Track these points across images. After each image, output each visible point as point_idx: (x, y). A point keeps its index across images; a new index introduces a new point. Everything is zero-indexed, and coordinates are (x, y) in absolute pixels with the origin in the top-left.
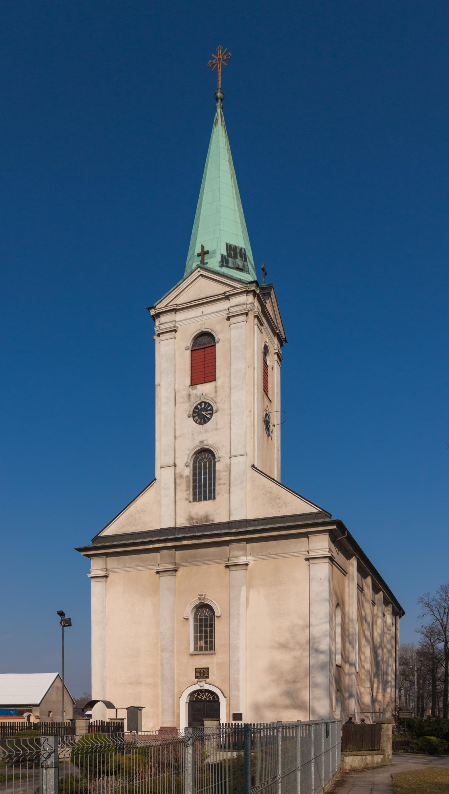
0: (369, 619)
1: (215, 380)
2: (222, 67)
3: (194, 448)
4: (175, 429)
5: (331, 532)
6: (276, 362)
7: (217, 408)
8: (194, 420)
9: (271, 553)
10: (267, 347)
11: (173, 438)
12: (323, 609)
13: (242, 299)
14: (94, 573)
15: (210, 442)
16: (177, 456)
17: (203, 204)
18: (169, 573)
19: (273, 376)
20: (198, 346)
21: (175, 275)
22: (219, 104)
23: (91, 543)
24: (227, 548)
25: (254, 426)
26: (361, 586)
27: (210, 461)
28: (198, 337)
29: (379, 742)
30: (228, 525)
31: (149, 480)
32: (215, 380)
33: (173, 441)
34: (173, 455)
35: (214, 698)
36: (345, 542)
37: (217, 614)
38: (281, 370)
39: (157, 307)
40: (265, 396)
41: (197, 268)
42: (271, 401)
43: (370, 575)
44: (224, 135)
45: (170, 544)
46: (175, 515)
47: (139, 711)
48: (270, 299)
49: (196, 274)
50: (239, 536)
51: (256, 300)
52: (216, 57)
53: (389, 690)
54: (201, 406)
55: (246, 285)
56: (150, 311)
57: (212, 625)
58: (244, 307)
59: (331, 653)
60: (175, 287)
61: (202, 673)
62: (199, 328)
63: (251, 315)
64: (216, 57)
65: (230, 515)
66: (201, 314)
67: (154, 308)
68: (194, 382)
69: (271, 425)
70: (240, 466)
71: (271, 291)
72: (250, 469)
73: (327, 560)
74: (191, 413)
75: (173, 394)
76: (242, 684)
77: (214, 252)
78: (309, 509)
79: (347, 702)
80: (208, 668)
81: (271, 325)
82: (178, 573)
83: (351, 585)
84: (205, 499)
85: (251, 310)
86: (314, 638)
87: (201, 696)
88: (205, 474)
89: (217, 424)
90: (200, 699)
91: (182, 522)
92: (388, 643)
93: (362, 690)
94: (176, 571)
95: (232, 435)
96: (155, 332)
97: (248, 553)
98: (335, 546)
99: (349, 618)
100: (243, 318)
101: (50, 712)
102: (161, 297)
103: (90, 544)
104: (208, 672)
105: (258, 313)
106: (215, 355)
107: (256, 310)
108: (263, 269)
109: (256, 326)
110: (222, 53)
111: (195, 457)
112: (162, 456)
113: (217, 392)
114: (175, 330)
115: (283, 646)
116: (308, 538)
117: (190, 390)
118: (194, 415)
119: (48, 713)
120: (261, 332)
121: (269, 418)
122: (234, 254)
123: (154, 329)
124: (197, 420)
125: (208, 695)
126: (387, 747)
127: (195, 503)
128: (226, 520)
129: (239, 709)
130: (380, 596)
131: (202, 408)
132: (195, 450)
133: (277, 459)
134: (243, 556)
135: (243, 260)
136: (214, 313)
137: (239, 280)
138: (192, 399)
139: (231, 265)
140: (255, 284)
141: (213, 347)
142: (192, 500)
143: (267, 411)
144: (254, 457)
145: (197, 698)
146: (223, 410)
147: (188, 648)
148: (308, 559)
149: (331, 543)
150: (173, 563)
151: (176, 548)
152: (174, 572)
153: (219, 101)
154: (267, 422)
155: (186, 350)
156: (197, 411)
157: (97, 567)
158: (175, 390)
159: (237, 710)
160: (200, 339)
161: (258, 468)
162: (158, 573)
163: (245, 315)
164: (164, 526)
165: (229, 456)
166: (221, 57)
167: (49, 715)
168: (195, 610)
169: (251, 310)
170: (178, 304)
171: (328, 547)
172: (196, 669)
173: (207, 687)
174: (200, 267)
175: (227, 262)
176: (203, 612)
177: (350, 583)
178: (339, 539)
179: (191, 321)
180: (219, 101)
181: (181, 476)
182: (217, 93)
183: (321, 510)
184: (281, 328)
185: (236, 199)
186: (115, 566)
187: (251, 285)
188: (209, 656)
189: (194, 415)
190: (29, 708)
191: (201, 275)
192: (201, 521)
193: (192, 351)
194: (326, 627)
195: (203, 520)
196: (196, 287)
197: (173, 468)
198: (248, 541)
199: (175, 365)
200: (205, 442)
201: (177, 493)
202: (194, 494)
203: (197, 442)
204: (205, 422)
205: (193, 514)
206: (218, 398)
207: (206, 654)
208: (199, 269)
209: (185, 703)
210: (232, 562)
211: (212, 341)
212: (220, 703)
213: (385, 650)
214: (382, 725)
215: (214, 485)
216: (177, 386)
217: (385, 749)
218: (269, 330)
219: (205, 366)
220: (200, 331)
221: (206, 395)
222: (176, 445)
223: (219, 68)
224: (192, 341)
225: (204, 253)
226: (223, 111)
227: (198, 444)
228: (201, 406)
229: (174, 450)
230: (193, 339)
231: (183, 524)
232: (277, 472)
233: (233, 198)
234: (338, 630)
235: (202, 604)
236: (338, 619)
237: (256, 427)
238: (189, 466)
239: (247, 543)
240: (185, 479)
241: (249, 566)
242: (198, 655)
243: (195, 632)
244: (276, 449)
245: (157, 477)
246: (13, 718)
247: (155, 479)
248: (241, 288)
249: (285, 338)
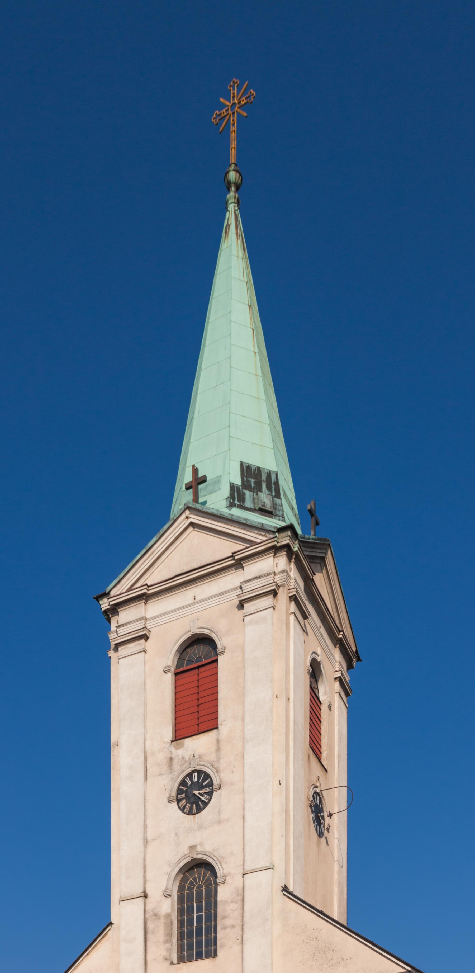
3: (179, 861)
4: (145, 826)
6: (337, 696)
7: (221, 781)
8: (179, 807)
10: (319, 663)
11: (141, 844)
15: (208, 848)
16: (149, 876)
17: (199, 392)
19: (331, 723)
20: (187, 665)
22: (232, 196)
25: (287, 811)
27: (208, 886)
28: (187, 647)
33: (142, 848)
34: (142, 874)
39: (113, 593)
40: (313, 759)
42: (326, 771)
44: (241, 253)
48: (324, 571)
49: (182, 523)
51: (293, 565)
52: (228, 103)
54: (191, 779)
55: (272, 536)
58: (269, 579)
63: (283, 595)
64: (228, 103)
66: (191, 601)
67: (106, 595)
68: (180, 734)
69: (326, 814)
70: (261, 891)
71: (326, 554)
72: (279, 895)
74: (174, 793)
75: (142, 758)
77: (218, 480)
84: (200, 956)
85: (283, 586)
88: (199, 910)
89: (219, 812)
95: (247, 831)
96: (110, 643)
100: (268, 601)
105: (297, 591)
109: (292, 617)
110: (238, 94)
111: (182, 878)
112: (123, 878)
114: (145, 634)
117: (173, 749)
118: (179, 796)
120: (305, 631)
121: (321, 801)
122: (255, 483)
124: (185, 806)
127: (182, 965)
131: (192, 783)
132: (182, 864)
133: (339, 883)
135: (274, 494)
136: (215, 596)
137: (260, 526)
138: (176, 767)
139: (248, 503)
140: (289, 533)
141: (215, 664)
142: (175, 960)
143: (316, 787)
144: (287, 872)
146: (232, 784)
153: (233, 189)
154: (317, 808)
156: (185, 789)
158: (145, 752)
160: (190, 651)
161: (296, 893)
163: (271, 596)
165: (242, 872)
166: (236, 101)
169: (283, 586)
170: (149, 584)
174: (188, 508)
175: (242, 498)
180: (233, 189)
182: (228, 172)
183: (409, 969)
185: (261, 379)
187: (283, 535)
191: (192, 524)
193: (176, 674)
196: (184, 547)
199: (145, 704)
200: (199, 849)
201: (148, 948)
202: (181, 948)
203: (184, 850)
206: (222, 761)
208: (187, 512)
215: (216, 932)
216: (148, 743)
218: (323, 630)
220: (189, 635)
221: (200, 756)
223: (233, 124)
228: (191, 779)
229: (143, 866)
230: (177, 651)
232: (339, 907)
237: (292, 813)
238: (170, 895)
240: (162, 920)
244: (336, 863)
245: (113, 919)
247: (111, 924)
249: (356, 650)
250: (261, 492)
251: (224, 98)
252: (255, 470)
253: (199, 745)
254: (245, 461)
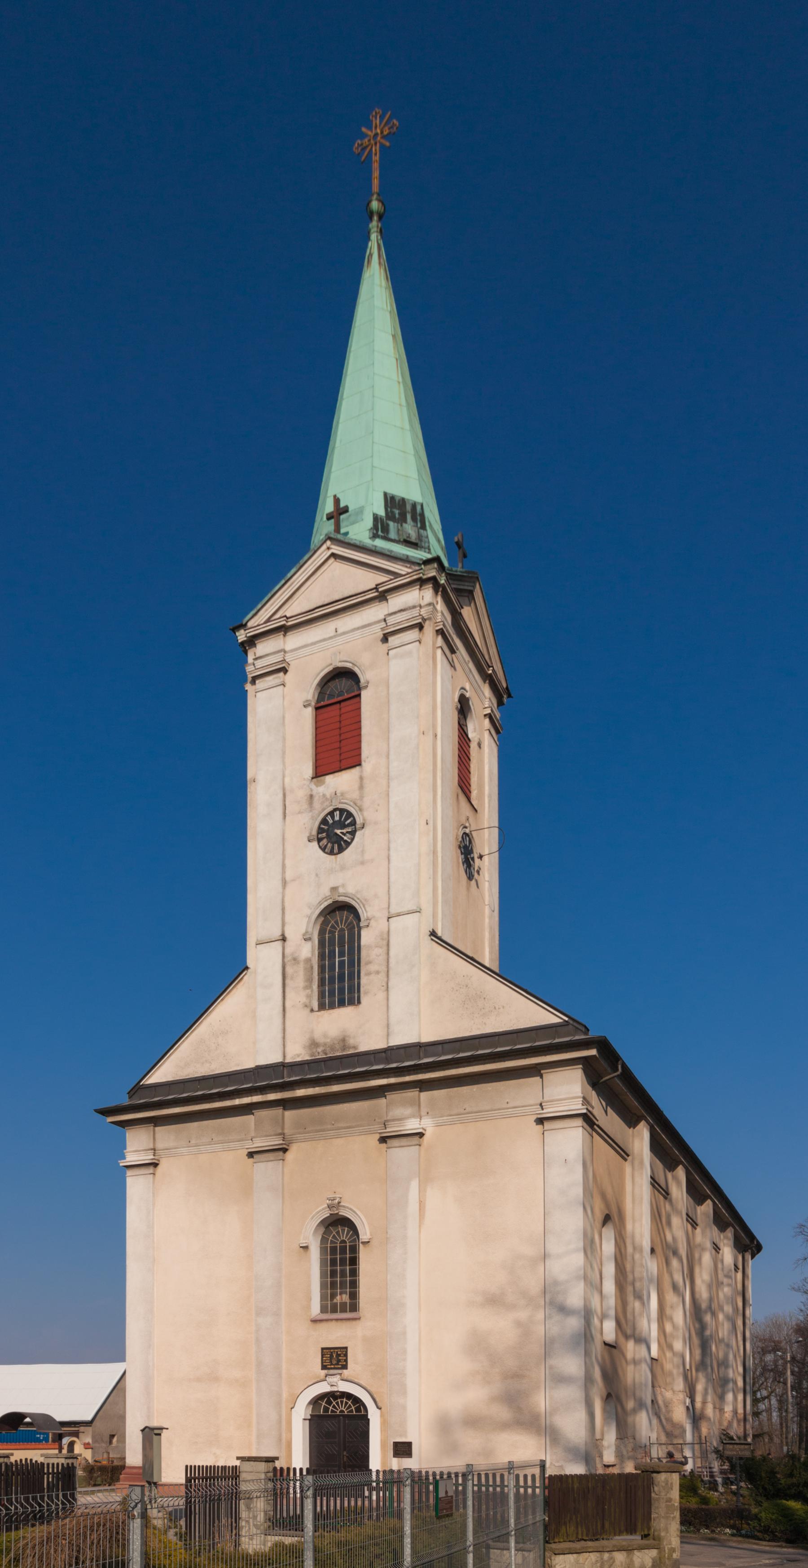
0: (683, 1252)
1: (360, 765)
2: (380, 151)
3: (320, 903)
5: (587, 1064)
6: (486, 734)
7: (364, 820)
8: (320, 847)
9: (467, 1111)
10: (467, 700)
12: (571, 1223)
13: (412, 596)
14: (131, 1158)
15: (351, 889)
16: (288, 918)
18: (271, 1156)
19: (481, 762)
21: (288, 549)
22: (374, 225)
23: (127, 1099)
24: (382, 1101)
25: (435, 852)
26: (664, 1187)
28: (329, 681)
29: (648, 1518)
30: (383, 1054)
31: (235, 968)
32: (360, 765)
33: (281, 890)
35: (358, 1410)
36: (619, 1088)
37: (363, 1237)
38: (499, 752)
39: (250, 624)
40: (462, 798)
41: (325, 542)
43: (681, 1163)
44: (384, 283)
45: (272, 1097)
46: (284, 1038)
47: (155, 1437)
48: (473, 604)
49: (322, 554)
50: (404, 1076)
51: (439, 599)
52: (369, 133)
53: (730, 1397)
54: (333, 817)
55: (417, 568)
56: (237, 634)
57: (354, 1261)
58: (415, 612)
59: (587, 1314)
60: (283, 582)
62: (329, 662)
63: (429, 629)
64: (369, 133)
65: (388, 1035)
66: (333, 633)
67: (243, 626)
68: (320, 771)
69: (476, 856)
70: (408, 934)
71: (474, 587)
72: (426, 940)
73: (579, 1122)
74: (314, 832)
75: (281, 796)
76: (411, 1381)
77: (361, 511)
78: (544, 1017)
79: (630, 1419)
80: (346, 1348)
81: (476, 656)
82: (289, 1156)
83: (637, 1179)
84: (342, 1004)
85: (430, 619)
86: (556, 1283)
87: (334, 1407)
88: (342, 954)
89: (363, 852)
90: (332, 1411)
91: (297, 1052)
92: (728, 1303)
93: (668, 1395)
94: (285, 1150)
95: (392, 872)
97: (423, 1111)
98: (598, 1095)
99: (633, 1243)
100: (413, 634)
101: (112, 1436)
102: (258, 603)
103: (126, 1101)
104: (346, 1355)
105: (444, 625)
106: (359, 715)
107: (439, 618)
108: (459, 545)
109: (439, 652)
110: (380, 123)
112: (260, 920)
113: (370, 793)
114: (284, 668)
115: (494, 1301)
116: (541, 1077)
117: (313, 786)
118: (320, 836)
119: (107, 1439)
121: (470, 842)
122: (399, 514)
123: (245, 671)
124: (326, 846)
125: (346, 1403)
126: (666, 1529)
127: (322, 1012)
128: (381, 1045)
129: (405, 1434)
130: (706, 1208)
131: (334, 822)
132: (323, 907)
133: (491, 928)
134: (414, 1116)
135: (419, 525)
136: (358, 628)
137: (405, 558)
138: (317, 805)
139: (393, 535)
140: (436, 565)
141: (357, 699)
142: (316, 1007)
143: (466, 827)
145: (326, 1410)
146: (376, 823)
147: (308, 1307)
148: (540, 1121)
149: (589, 1088)
150: (280, 1134)
151: (285, 1104)
152: (281, 1153)
153: (375, 218)
154: (466, 850)
155: (305, 706)
156: (326, 827)
157: (137, 1145)
159: (401, 1436)
161: (444, 938)
162: (251, 1155)
163: (417, 630)
164: (263, 1061)
165: (387, 915)
166: (379, 131)
167: (111, 1442)
168: (322, 1230)
169: (430, 619)
170: (288, 615)
171: (580, 1095)
172: (323, 1349)
173: (344, 1387)
174: (330, 538)
175: (386, 529)
176: (338, 1233)
177: (636, 1174)
178: (604, 1079)
179: (315, 648)
180: (375, 218)
181: (295, 960)
183: (566, 1019)
184: (497, 666)
186: (171, 1144)
187: (429, 567)
188: (348, 1324)
189: (320, 836)
190: (74, 1427)
191: (333, 555)
192: (332, 1048)
194: (578, 1259)
195: (337, 1047)
196: (325, 578)
197: (280, 943)
198: (424, 1086)
199: (284, 739)
200: (341, 890)
202: (321, 995)
203: (325, 891)
204: (341, 850)
205: (318, 1036)
207: (341, 1320)
208: (329, 543)
209: (301, 1420)
210: (392, 1129)
211: (355, 687)
212: (369, 1420)
213: (721, 1317)
214: (655, 1475)
215: (359, 977)
216: (287, 780)
217: (663, 1534)
218: (471, 665)
219: (343, 737)
220: (330, 668)
221: (342, 794)
222: (286, 899)
223: (376, 154)
224: (316, 689)
225: (340, 511)
226: (382, 237)
227: (328, 893)
230: (318, 685)
231: (298, 1056)
232: (491, 953)
233: (400, 405)
234: (610, 1269)
235: (335, 1218)
236: (608, 1247)
237: (440, 854)
238: (309, 939)
239: (421, 1091)
240: (302, 965)
241: (425, 1137)
242: (327, 1320)
243: (323, 1275)
245: (249, 963)
246: (41, 1447)
247: (247, 968)
248: (408, 573)
249: (507, 688)
251: (367, 127)
252: (399, 501)
253: (341, 784)
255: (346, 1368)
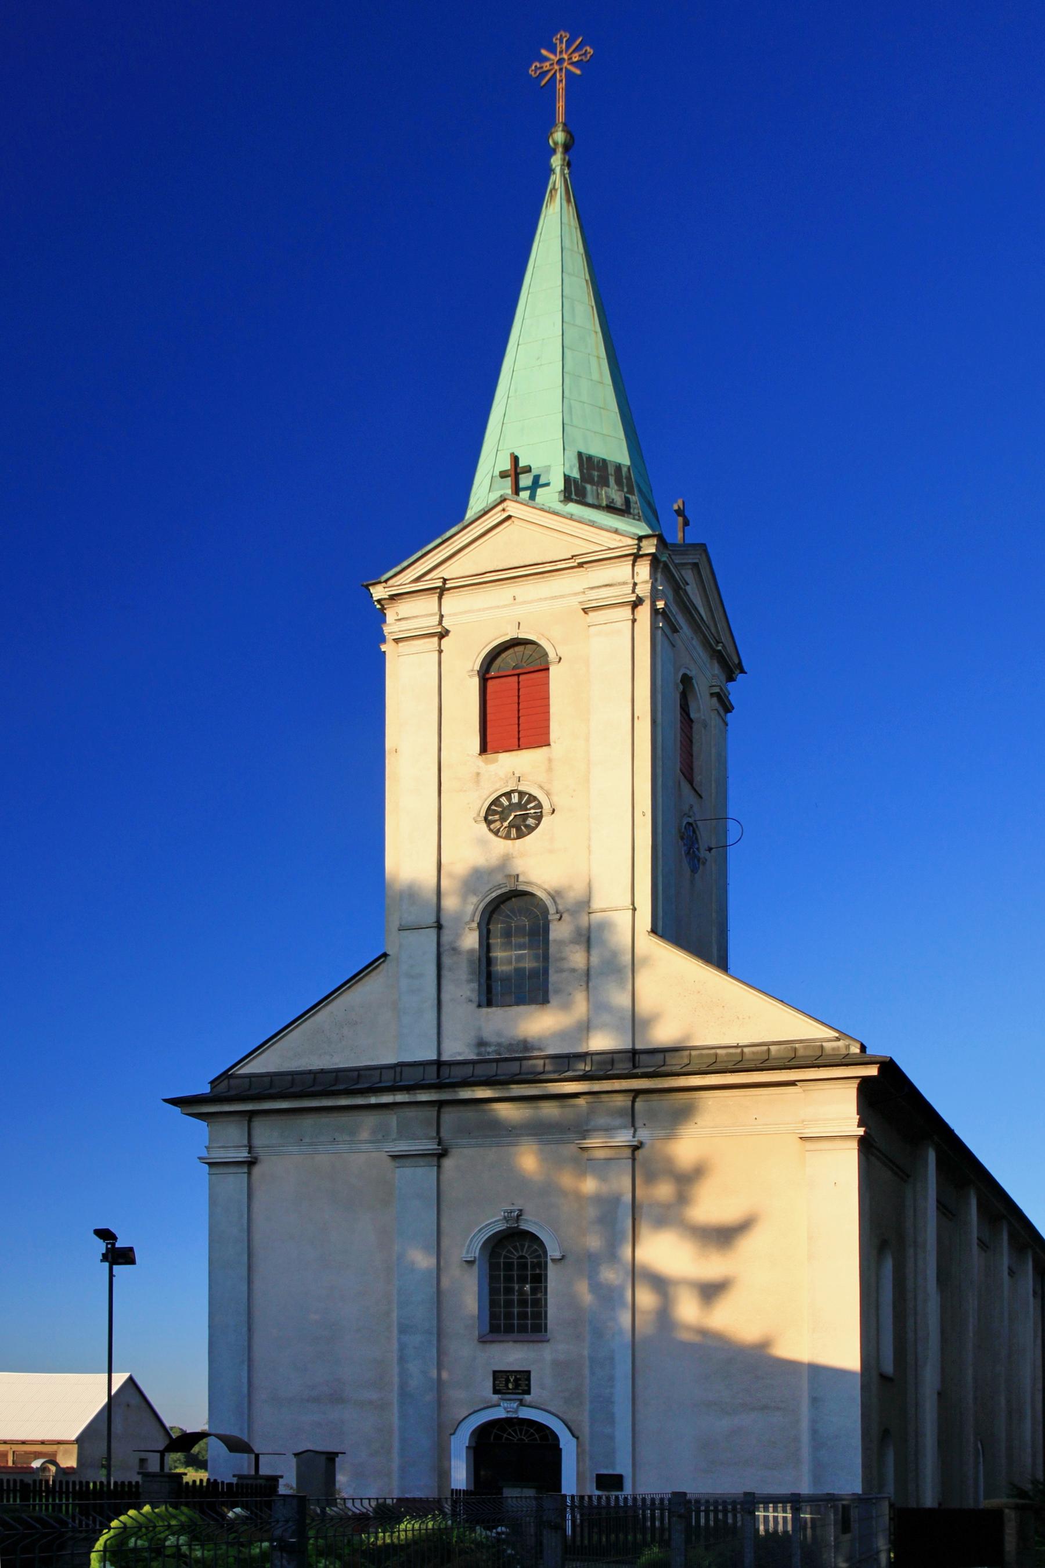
3: (491, 891)
18: (421, 1161)
21: (435, 506)
28: (492, 912)
42: (701, 797)
52: (552, 56)
54: (509, 799)
60: (439, 541)
61: (513, 1383)
73: (443, 641)
74: (483, 814)
104: (529, 1379)
109: (660, 632)
121: (694, 832)
131: (511, 804)
132: (494, 895)
136: (546, 599)
139: (590, 500)
162: (394, 1157)
173: (525, 1413)
181: (455, 950)
205: (488, 1035)
212: (561, 1450)
223: (561, 81)
231: (460, 1054)
233: (598, 357)
250: (608, 486)
251: (574, 74)
252: (599, 462)
254: (583, 450)
255: (529, 1393)
